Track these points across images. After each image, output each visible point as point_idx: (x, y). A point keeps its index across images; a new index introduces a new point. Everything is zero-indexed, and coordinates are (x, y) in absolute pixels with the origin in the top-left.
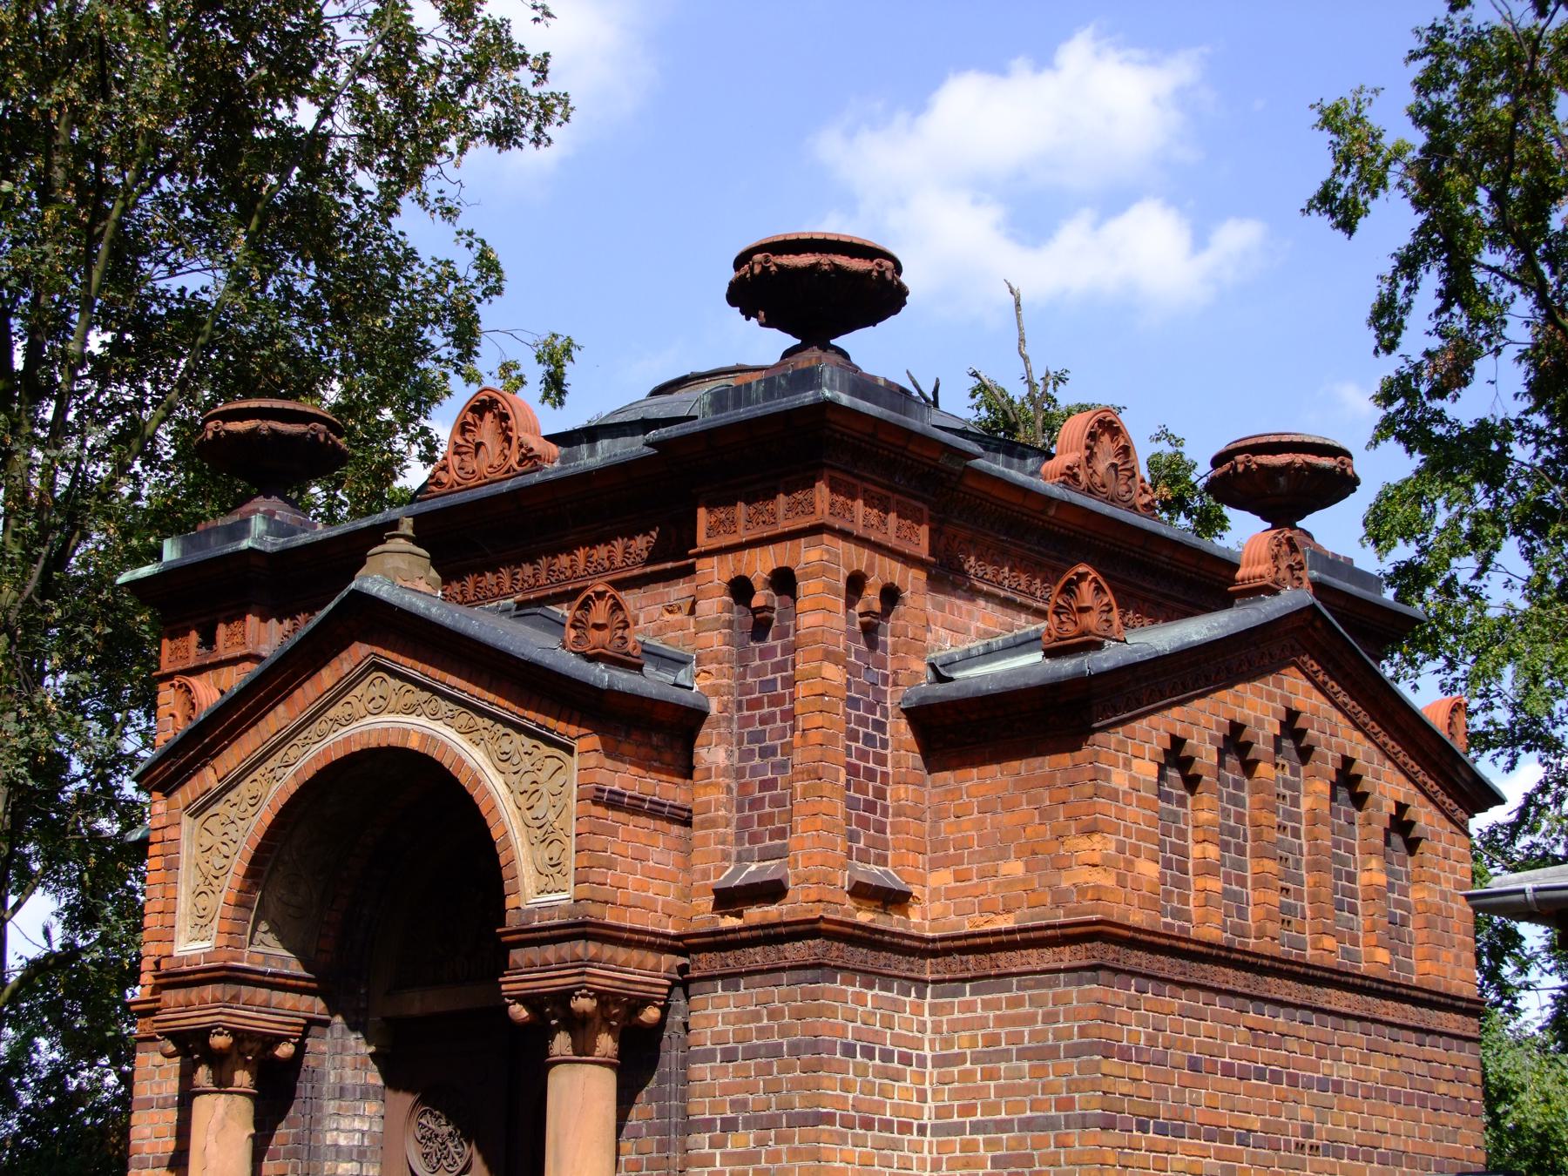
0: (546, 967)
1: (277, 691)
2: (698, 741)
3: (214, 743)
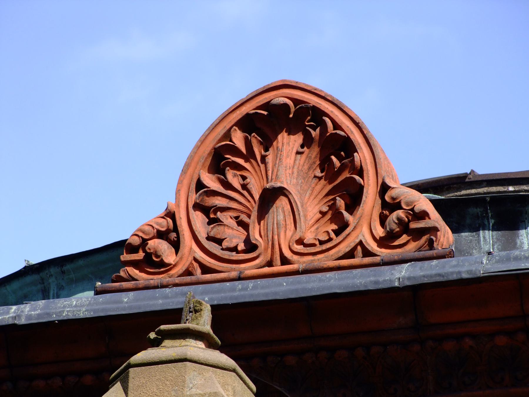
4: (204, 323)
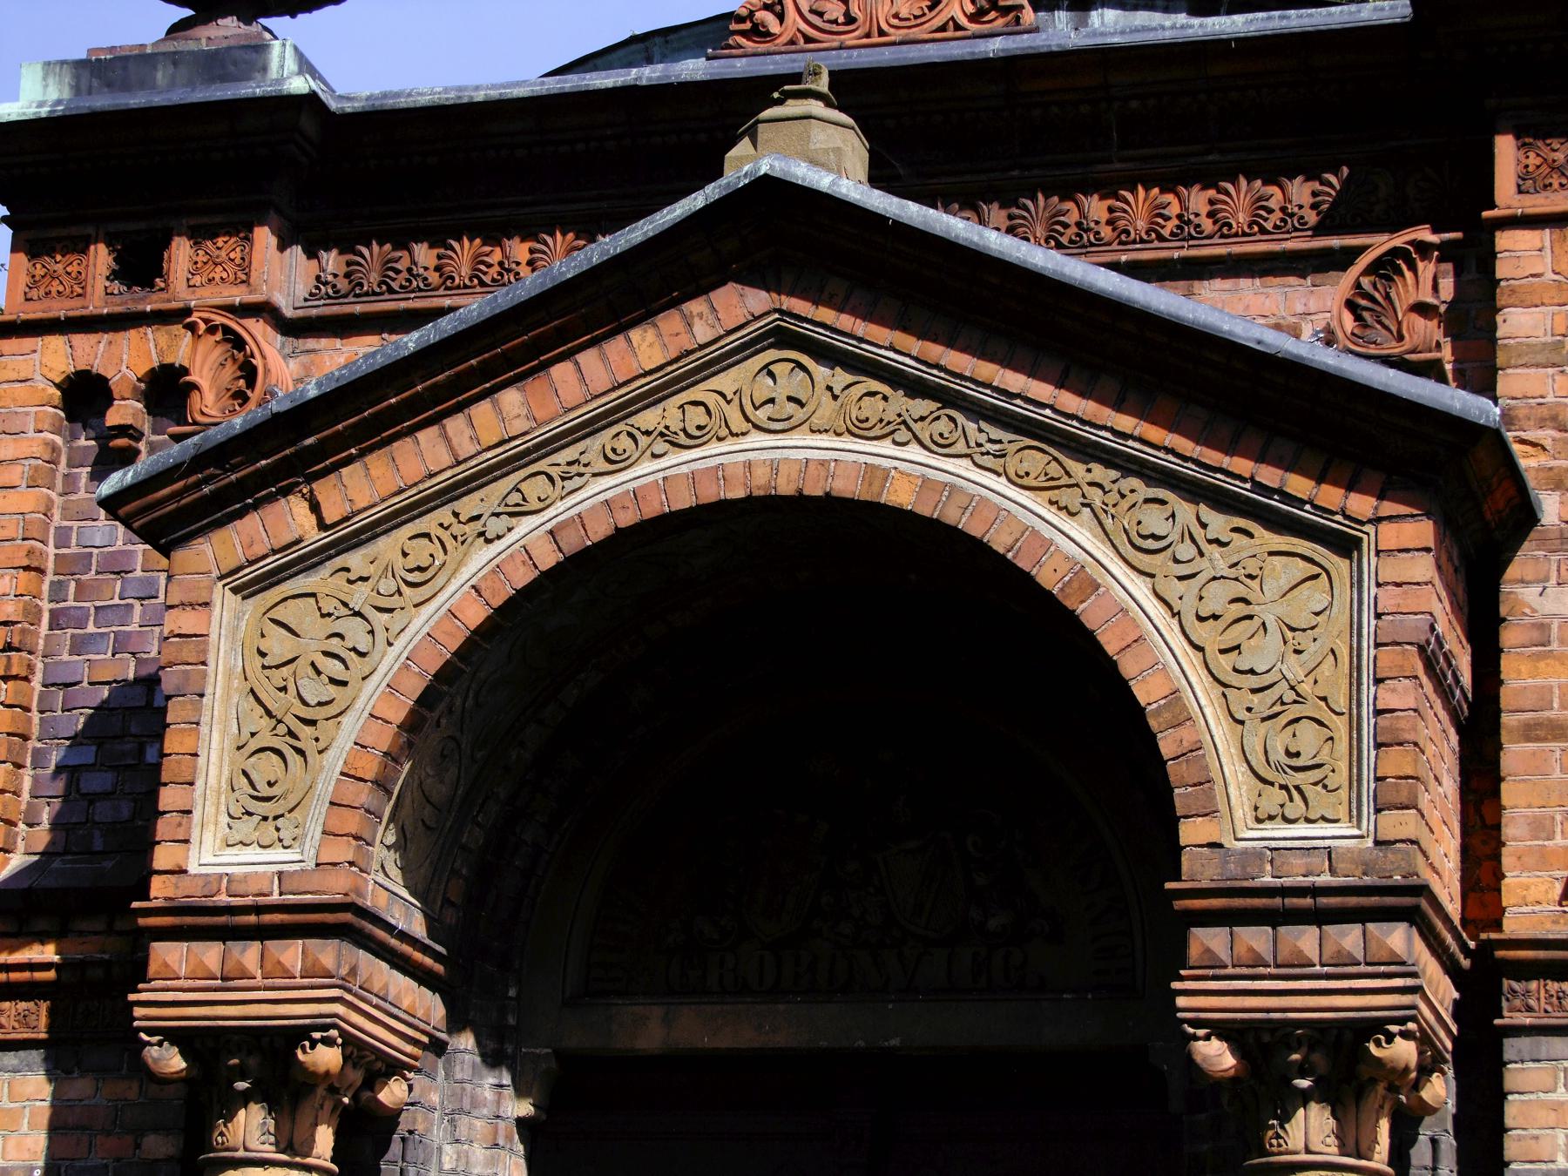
0: (1296, 966)
1: (509, 361)
2: (1512, 571)
3: (320, 452)
4: (823, 85)
